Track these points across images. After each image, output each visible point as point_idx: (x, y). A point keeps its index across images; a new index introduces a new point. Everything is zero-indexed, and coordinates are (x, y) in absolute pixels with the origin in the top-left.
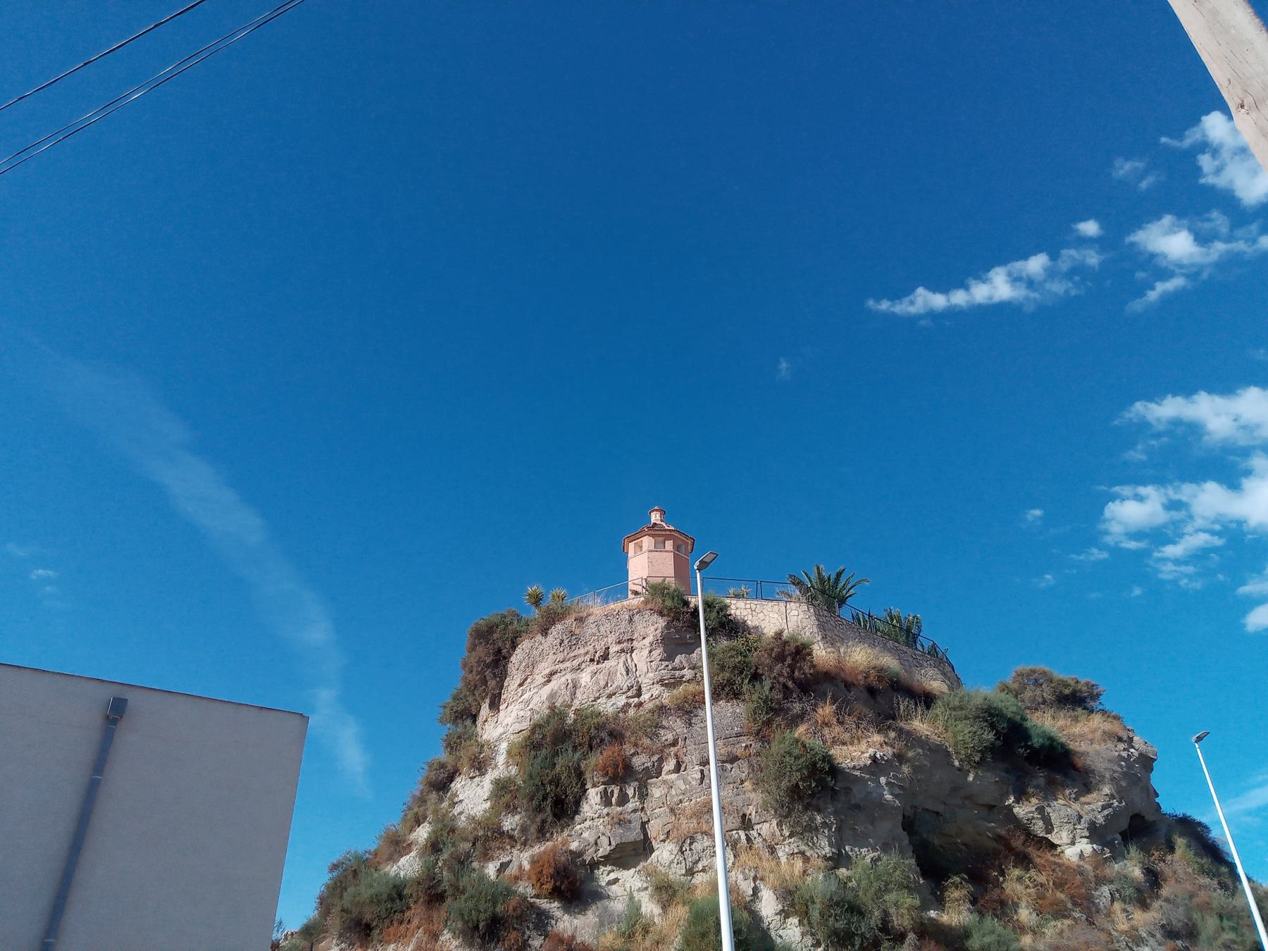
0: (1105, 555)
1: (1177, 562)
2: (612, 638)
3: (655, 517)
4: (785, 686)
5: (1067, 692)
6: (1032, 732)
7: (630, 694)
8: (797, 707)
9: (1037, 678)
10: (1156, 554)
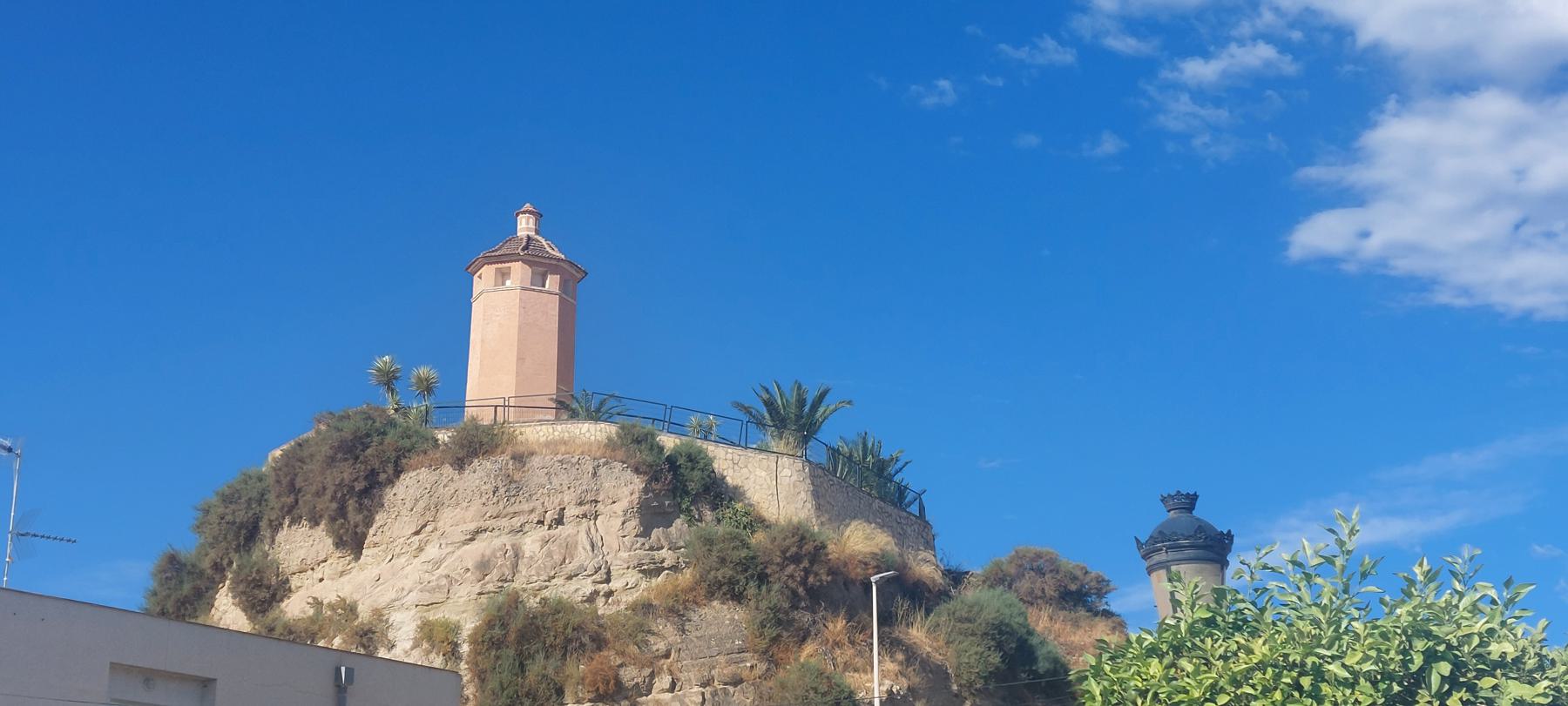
0: (1068, 57)
1: (1200, 95)
2: (568, 497)
3: (525, 225)
4: (794, 593)
5: (1073, 587)
6: (1041, 652)
7: (597, 577)
8: (805, 618)
9: (1039, 565)
10: (1166, 74)
